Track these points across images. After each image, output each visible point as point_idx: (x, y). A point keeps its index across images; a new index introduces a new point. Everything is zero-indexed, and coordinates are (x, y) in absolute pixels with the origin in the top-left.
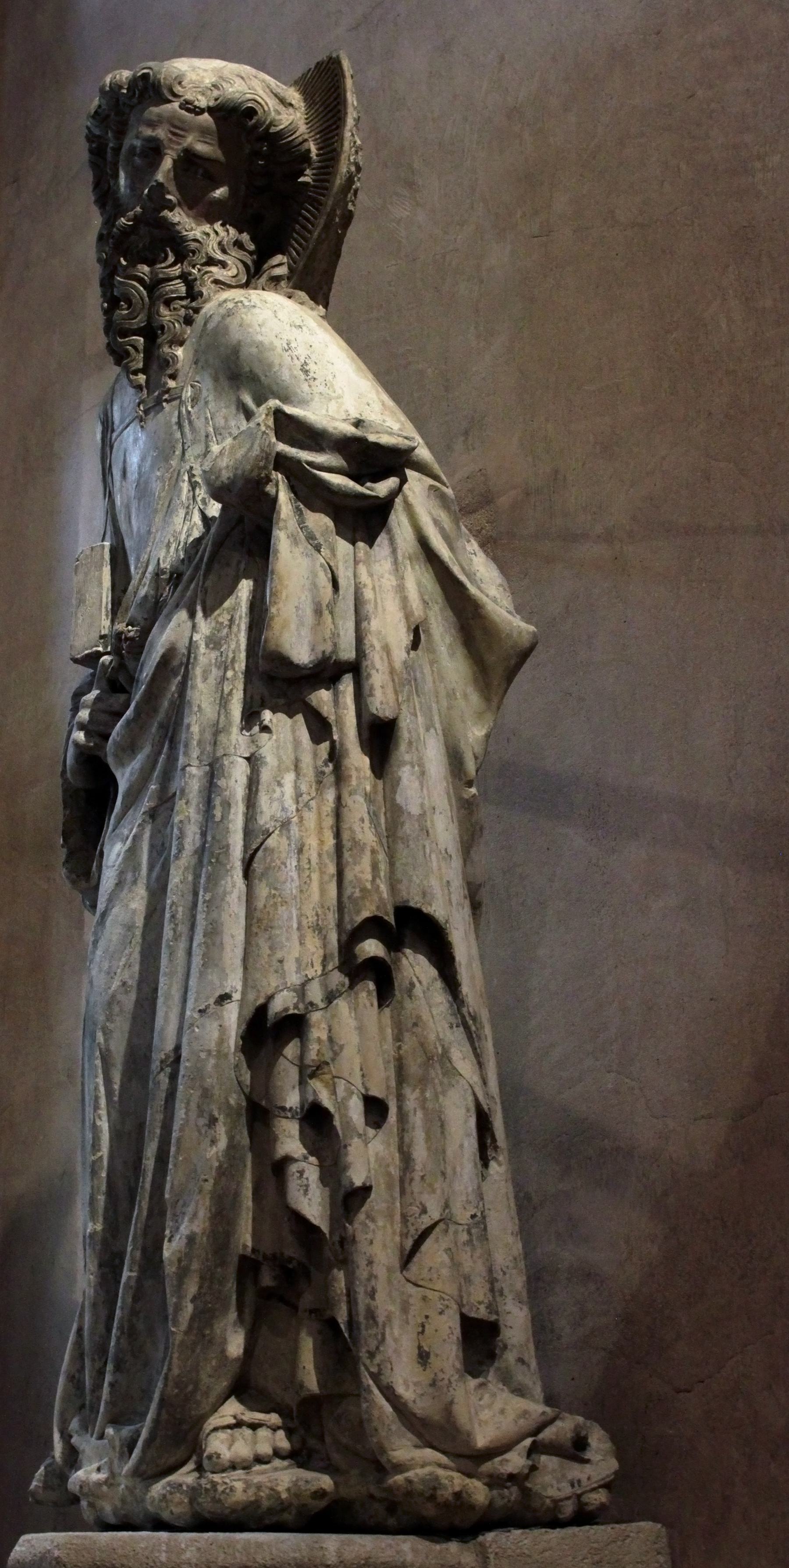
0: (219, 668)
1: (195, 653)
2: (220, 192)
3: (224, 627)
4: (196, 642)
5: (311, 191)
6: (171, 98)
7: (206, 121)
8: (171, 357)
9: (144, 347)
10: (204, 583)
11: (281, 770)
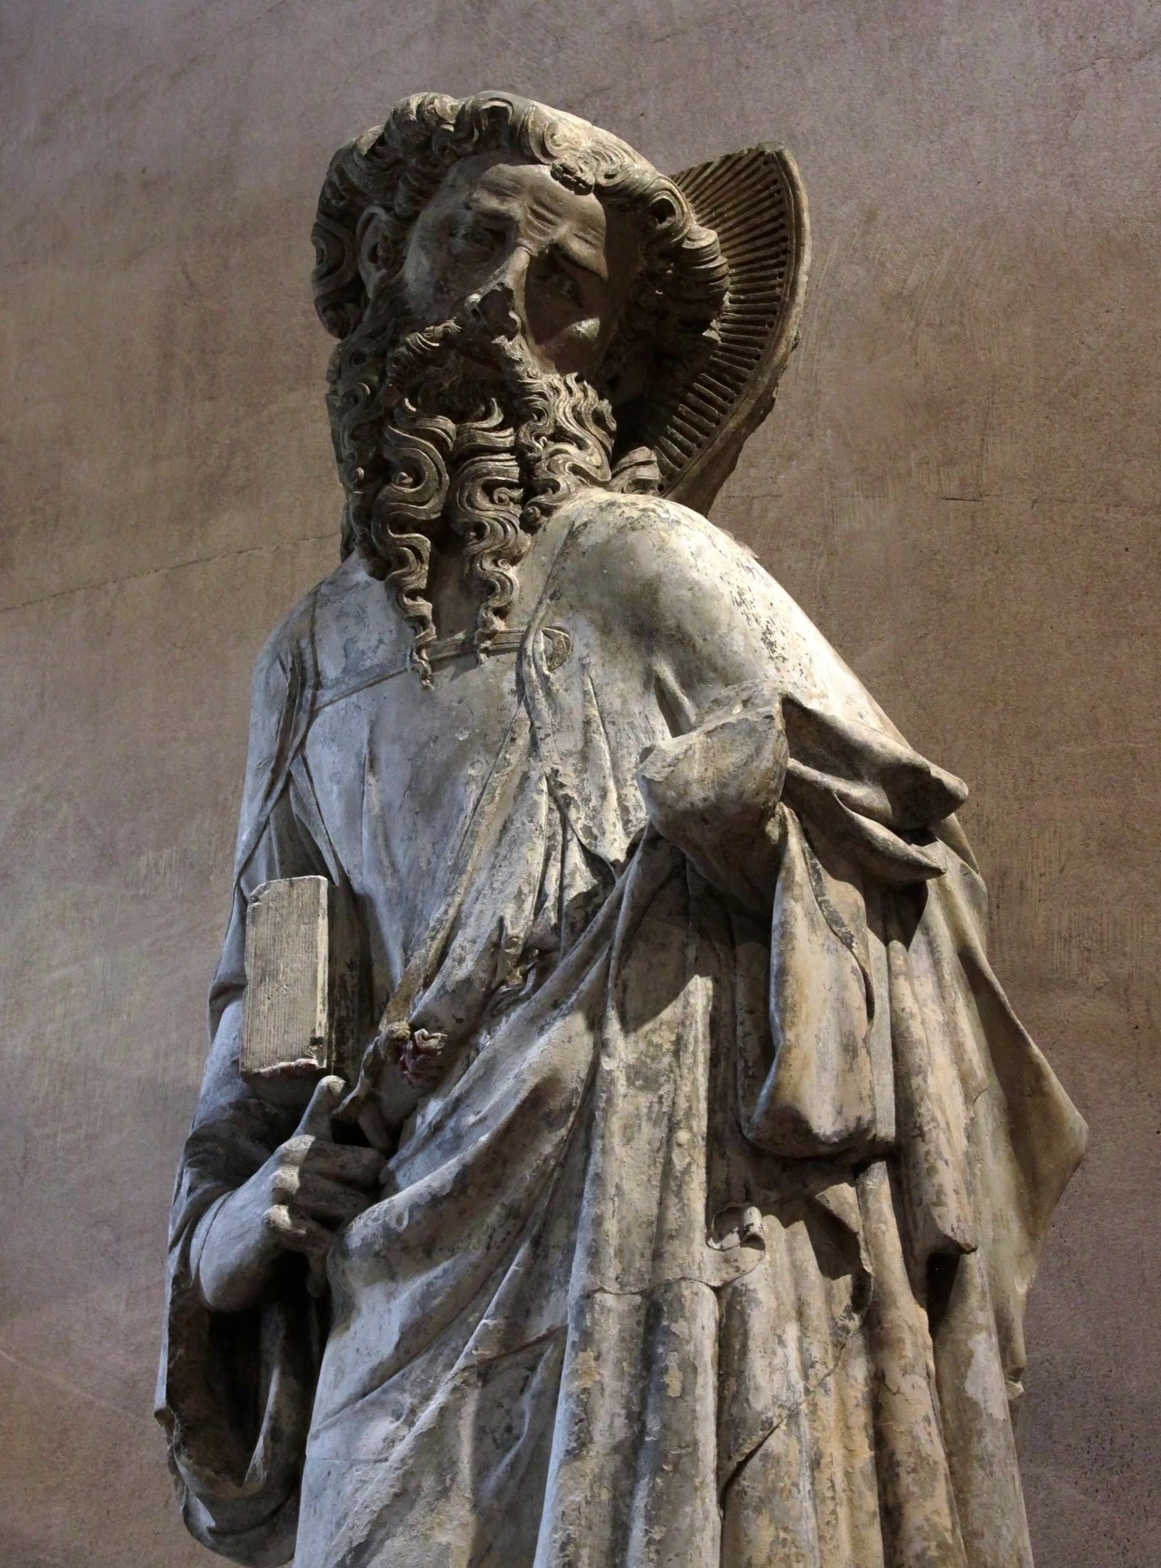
0: (656, 1124)
1: (609, 1091)
2: (588, 326)
3: (664, 1054)
4: (610, 1072)
5: (716, 356)
6: (538, 156)
7: (592, 206)
8: (499, 580)
9: (431, 554)
10: (619, 971)
11: (780, 1317)
